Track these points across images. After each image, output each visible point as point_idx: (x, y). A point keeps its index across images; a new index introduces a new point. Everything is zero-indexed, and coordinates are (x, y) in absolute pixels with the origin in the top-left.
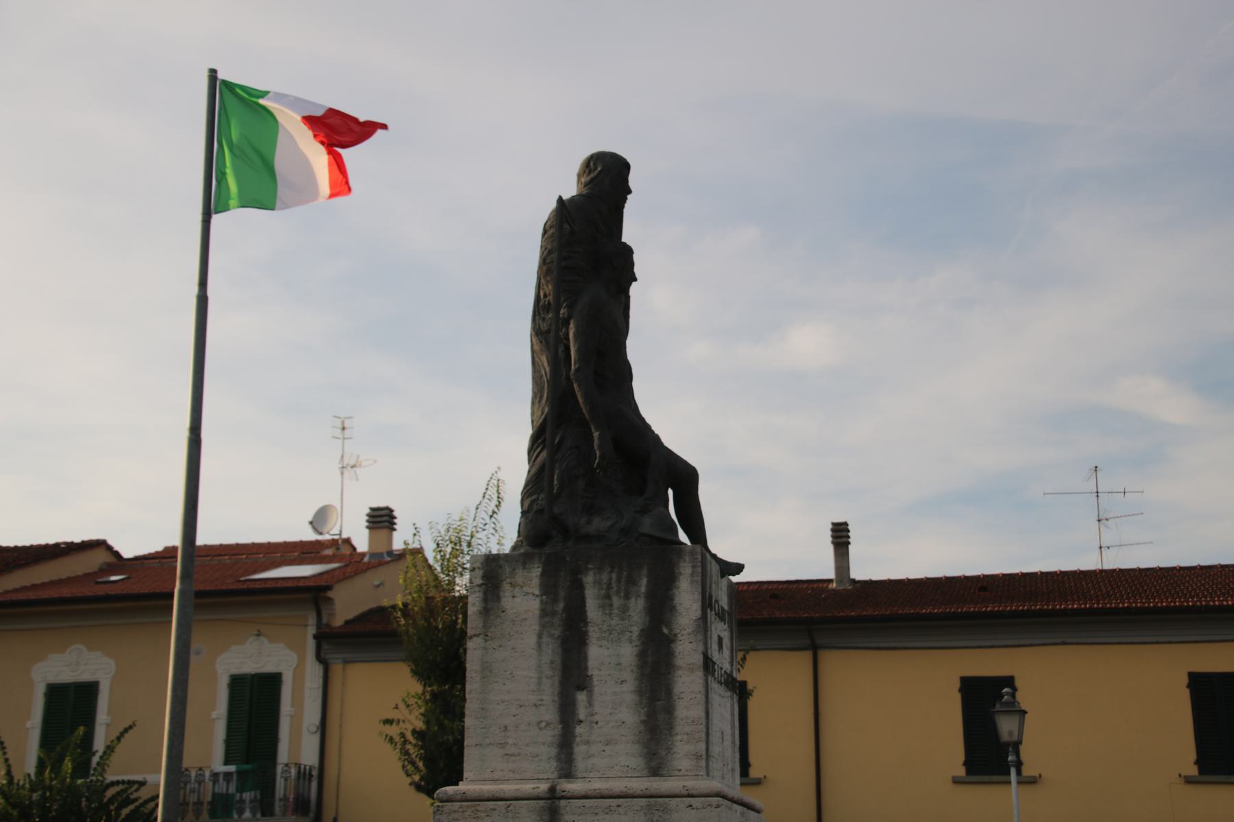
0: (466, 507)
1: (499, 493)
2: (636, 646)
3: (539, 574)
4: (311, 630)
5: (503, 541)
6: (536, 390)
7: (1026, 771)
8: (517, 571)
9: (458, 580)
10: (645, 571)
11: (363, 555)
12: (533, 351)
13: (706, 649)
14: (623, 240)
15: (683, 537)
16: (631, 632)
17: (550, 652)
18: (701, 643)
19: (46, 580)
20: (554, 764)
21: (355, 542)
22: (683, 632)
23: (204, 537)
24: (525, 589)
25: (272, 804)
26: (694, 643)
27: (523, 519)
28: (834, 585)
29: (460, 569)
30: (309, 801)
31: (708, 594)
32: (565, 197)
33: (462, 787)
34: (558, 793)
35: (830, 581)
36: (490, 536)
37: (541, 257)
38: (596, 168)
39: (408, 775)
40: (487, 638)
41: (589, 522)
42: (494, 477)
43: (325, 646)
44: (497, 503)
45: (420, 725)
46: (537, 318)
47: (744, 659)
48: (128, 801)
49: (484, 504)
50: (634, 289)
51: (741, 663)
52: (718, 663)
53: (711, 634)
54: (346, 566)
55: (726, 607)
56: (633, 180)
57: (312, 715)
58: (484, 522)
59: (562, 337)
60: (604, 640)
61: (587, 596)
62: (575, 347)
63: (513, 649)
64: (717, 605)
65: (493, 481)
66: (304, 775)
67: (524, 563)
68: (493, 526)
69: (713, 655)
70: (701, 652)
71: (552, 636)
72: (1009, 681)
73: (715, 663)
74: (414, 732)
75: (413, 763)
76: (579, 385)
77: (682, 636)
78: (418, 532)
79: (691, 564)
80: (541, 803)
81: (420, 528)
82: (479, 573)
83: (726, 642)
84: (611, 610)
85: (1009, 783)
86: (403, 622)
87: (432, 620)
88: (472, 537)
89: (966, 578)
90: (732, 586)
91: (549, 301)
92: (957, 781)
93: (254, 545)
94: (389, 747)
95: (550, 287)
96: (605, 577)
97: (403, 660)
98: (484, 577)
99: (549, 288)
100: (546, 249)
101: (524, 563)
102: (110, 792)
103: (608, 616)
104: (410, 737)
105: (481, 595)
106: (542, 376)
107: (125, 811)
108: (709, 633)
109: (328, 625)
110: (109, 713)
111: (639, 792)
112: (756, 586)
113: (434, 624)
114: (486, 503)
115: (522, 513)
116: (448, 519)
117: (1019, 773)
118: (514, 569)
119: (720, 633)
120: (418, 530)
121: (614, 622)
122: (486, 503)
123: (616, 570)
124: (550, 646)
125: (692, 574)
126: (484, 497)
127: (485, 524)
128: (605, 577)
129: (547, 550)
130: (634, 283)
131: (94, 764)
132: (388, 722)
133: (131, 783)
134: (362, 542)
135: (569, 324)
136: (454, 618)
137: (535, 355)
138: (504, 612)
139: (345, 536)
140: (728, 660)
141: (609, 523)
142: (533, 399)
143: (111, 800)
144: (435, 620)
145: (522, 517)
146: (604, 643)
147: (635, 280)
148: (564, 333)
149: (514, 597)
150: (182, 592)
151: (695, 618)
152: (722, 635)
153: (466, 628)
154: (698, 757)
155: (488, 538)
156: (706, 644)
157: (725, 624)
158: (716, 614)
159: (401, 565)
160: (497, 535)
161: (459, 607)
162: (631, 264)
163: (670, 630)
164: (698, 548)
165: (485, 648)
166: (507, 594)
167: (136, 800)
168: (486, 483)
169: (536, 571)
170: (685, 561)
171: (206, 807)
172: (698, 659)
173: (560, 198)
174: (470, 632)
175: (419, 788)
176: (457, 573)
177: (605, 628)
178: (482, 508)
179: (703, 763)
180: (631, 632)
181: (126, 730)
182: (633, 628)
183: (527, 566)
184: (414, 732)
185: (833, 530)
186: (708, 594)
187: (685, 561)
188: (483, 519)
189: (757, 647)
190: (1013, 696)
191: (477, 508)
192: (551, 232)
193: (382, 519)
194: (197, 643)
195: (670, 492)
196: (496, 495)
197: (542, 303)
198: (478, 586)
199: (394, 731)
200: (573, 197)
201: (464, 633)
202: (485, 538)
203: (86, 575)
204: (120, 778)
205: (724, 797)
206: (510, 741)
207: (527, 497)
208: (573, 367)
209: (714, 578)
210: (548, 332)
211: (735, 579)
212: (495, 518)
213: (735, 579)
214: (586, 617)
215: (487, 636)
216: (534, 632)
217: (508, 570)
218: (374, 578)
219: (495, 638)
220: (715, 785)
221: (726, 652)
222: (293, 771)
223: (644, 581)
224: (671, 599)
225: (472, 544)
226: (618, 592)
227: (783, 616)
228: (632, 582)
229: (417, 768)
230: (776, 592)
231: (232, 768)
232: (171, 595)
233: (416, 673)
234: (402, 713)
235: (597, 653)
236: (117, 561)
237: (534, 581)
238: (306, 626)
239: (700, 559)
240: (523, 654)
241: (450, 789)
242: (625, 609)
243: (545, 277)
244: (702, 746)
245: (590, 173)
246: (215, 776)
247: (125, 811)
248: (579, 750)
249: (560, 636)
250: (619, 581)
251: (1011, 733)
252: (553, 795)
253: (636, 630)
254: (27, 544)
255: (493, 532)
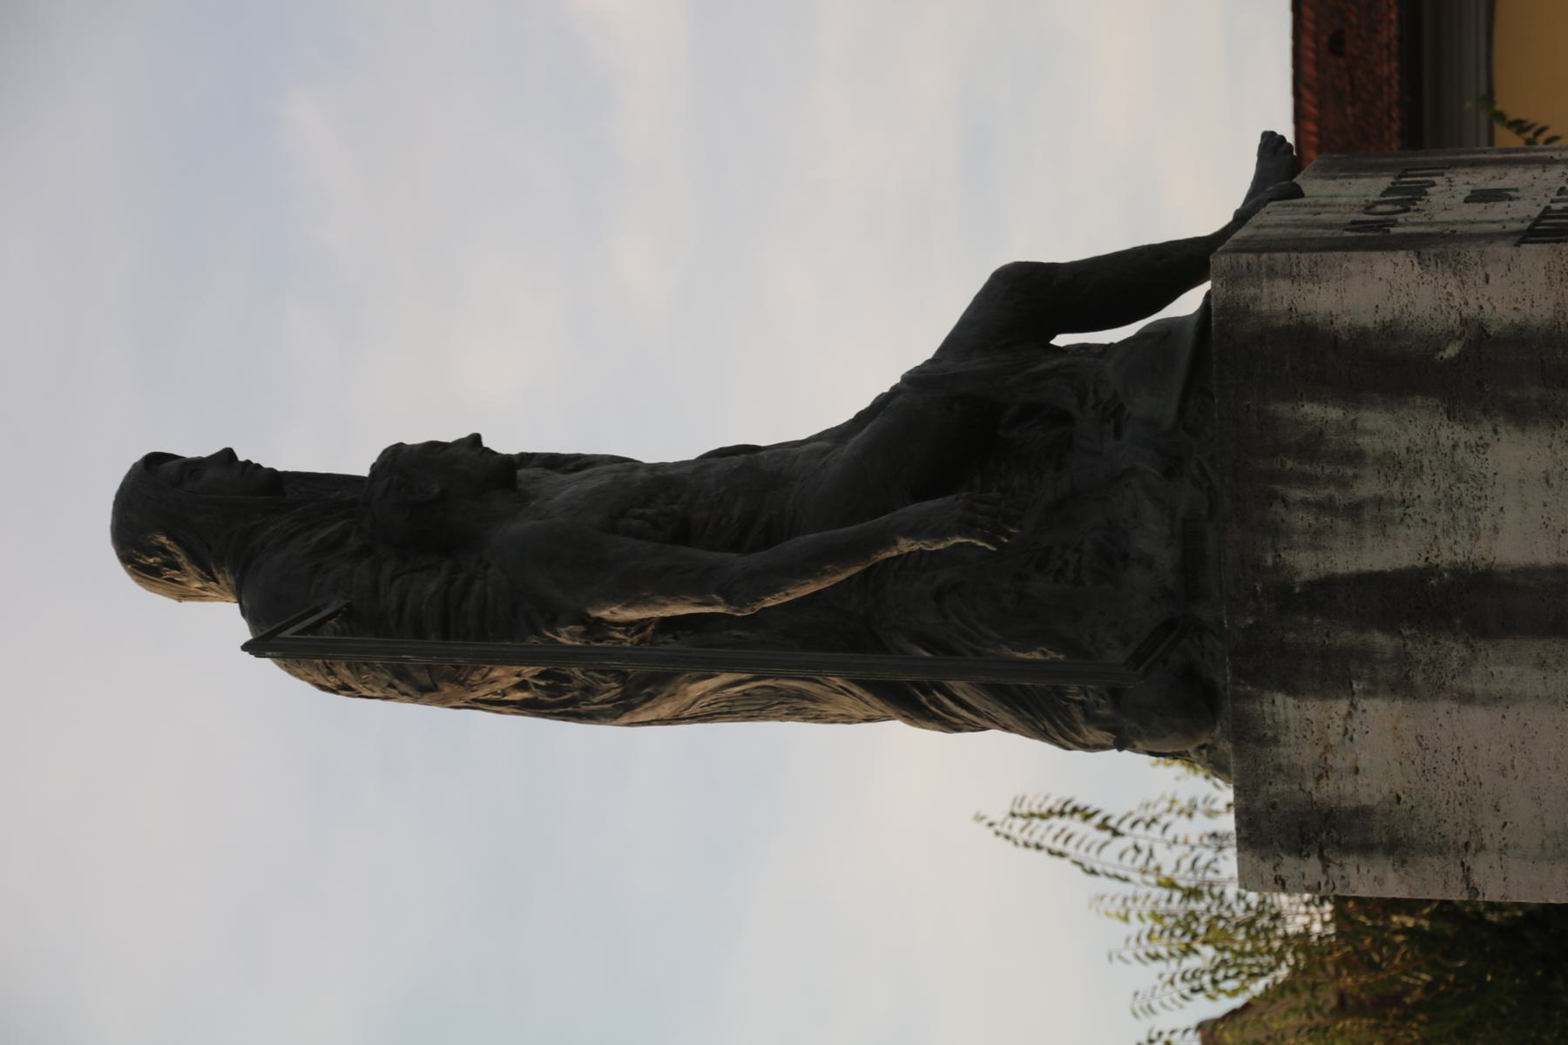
0: (1090, 906)
1: (1050, 813)
2: (1495, 431)
3: (1290, 701)
5: (1183, 802)
6: (784, 709)
8: (1284, 762)
9: (1295, 925)
10: (1283, 409)
13: (1505, 235)
14: (365, 472)
15: (1188, 303)
16: (1455, 446)
17: (1511, 671)
18: (1489, 249)
22: (1457, 301)
24: (1334, 739)
26: (1489, 270)
27: (1139, 745)
29: (1265, 921)
31: (1348, 234)
32: (247, 636)
36: (1169, 835)
37: (415, 700)
38: (162, 549)
40: (1473, 845)
42: (1005, 830)
44: (1077, 817)
46: (584, 708)
47: (1519, 126)
49: (1080, 854)
50: (503, 442)
51: (1530, 135)
52: (1546, 202)
53: (1464, 223)
55: (1386, 181)
56: (195, 445)
58: (1132, 853)
59: (636, 638)
60: (1477, 519)
61: (1353, 568)
62: (664, 605)
63: (1503, 772)
64: (1380, 208)
65: (1015, 832)
67: (1261, 741)
68: (1140, 827)
69: (1523, 215)
70: (1514, 250)
71: (1465, 666)
73: (1548, 208)
76: (770, 592)
77: (1466, 303)
78: (1160, 1034)
79: (1265, 283)
81: (1150, 1032)
82: (1290, 866)
83: (1484, 179)
84: (1392, 502)
87: (1408, 1000)
88: (1171, 885)
91: (541, 676)
95: (497, 673)
96: (1301, 520)
98: (1300, 852)
99: (504, 677)
100: (391, 686)
101: (1261, 741)
103: (1410, 511)
105: (1351, 861)
106: (745, 694)
108: (1459, 228)
112: (1307, 95)
113: (1417, 993)
114: (1078, 846)
115: (1120, 749)
116: (1127, 962)
118: (1279, 768)
119: (1461, 198)
120: (1154, 1036)
121: (1427, 494)
122: (1078, 846)
123: (1278, 487)
124: (1495, 669)
125: (1293, 277)
126: (1061, 855)
127: (1137, 849)
128: (1301, 520)
130: (486, 443)
135: (600, 620)
136: (1400, 938)
137: (686, 714)
138: (1399, 798)
140: (1537, 172)
142: (805, 720)
144: (1408, 988)
145: (1134, 749)
146: (1485, 521)
147: (476, 439)
148: (625, 632)
149: (1357, 770)
151: (1417, 268)
152: (1466, 191)
153: (1429, 902)
155: (1175, 842)
156: (1490, 237)
157: (1433, 184)
158: (1407, 210)
160: (1164, 820)
161: (1369, 923)
163: (1450, 336)
164: (1219, 261)
165: (1503, 850)
166: (1349, 789)
168: (1022, 851)
169: (1284, 708)
170: (1255, 299)
173: (247, 647)
174: (1457, 894)
176: (1275, 927)
177: (1443, 518)
178: (1091, 859)
180: (1455, 446)
182: (1443, 440)
183: (1270, 733)
186: (1348, 234)
187: (1255, 299)
188: (1121, 856)
189: (1483, 90)
191: (1093, 872)
192: (345, 674)
195: (1061, 340)
196: (1055, 820)
197: (542, 696)
198: (1325, 870)
200: (243, 613)
201: (1445, 910)
202: (1179, 850)
207: (1079, 733)
208: (720, 610)
209: (1302, 215)
210: (622, 676)
212: (1120, 822)
214: (1413, 570)
215: (1467, 845)
216: (1455, 715)
217: (1279, 787)
219: (1473, 823)
221: (1513, 178)
223: (1312, 411)
224: (1362, 334)
225: (1193, 884)
226: (1343, 484)
227: (1393, 17)
228: (1312, 445)
230: (1325, 39)
237: (1311, 714)
239: (1251, 257)
240: (1518, 744)
242: (1390, 464)
243: (471, 688)
245: (177, 567)
249: (1466, 643)
250: (1308, 481)
253: (1450, 433)
255: (1156, 829)
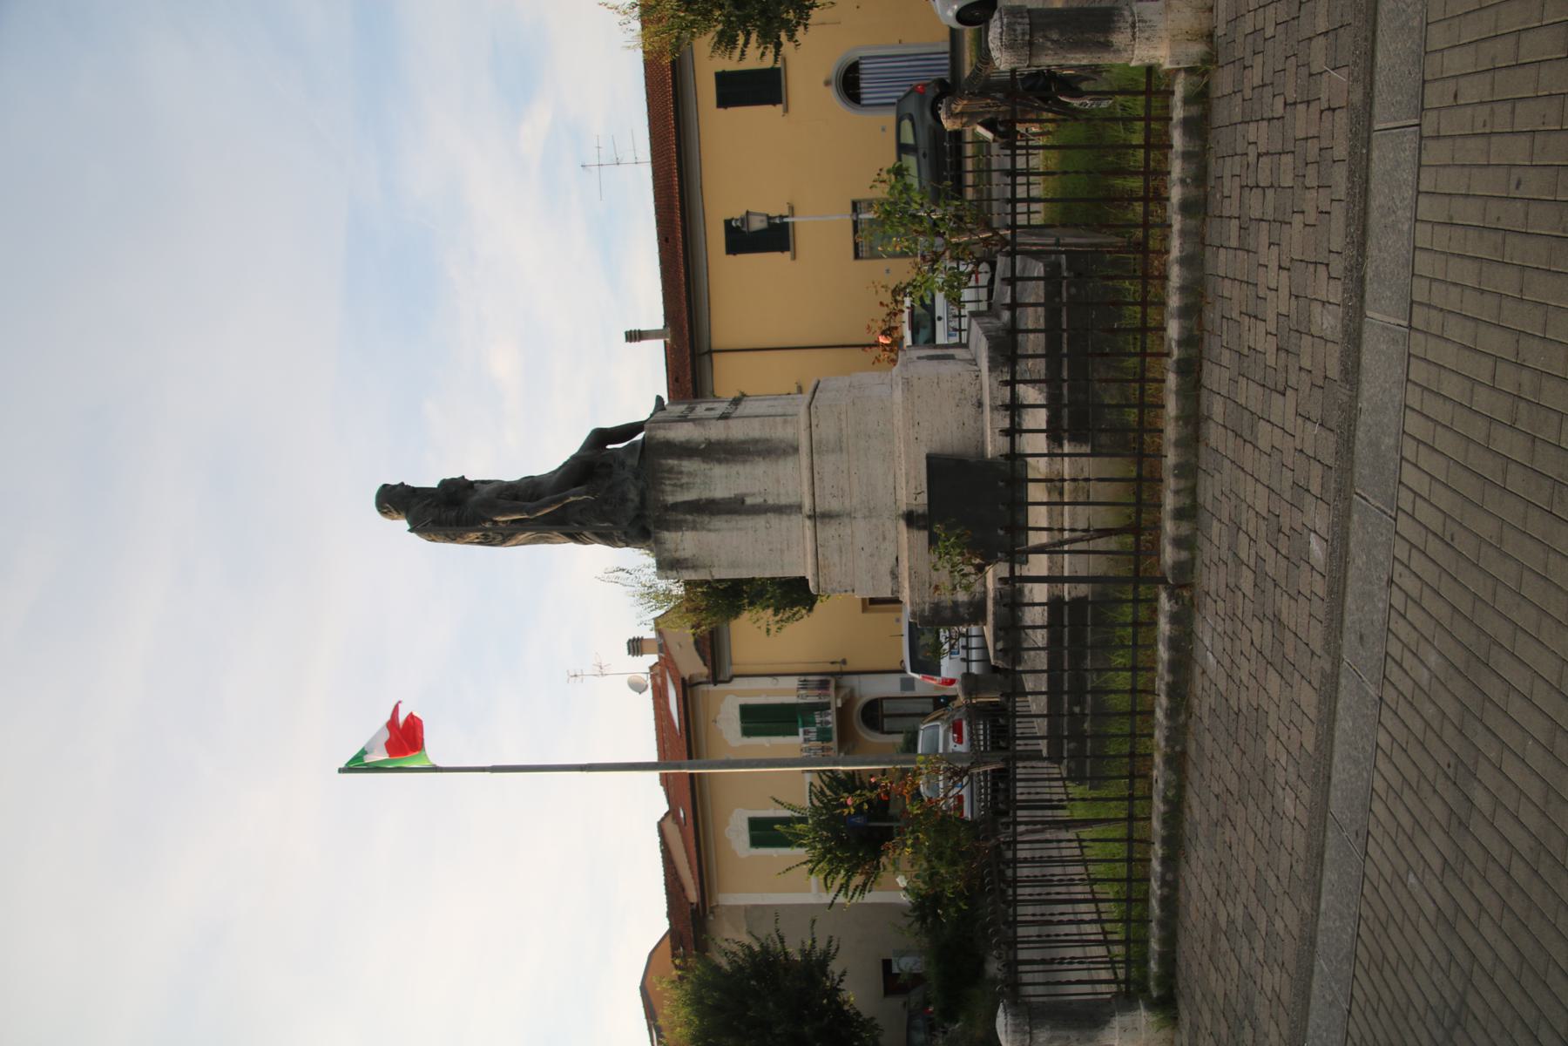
4: (711, 687)
7: (786, 212)
10: (663, 462)
11: (660, 658)
12: (516, 545)
15: (639, 437)
19: (684, 855)
20: (793, 517)
21: (652, 664)
23: (653, 757)
25: (823, 703)
28: (668, 340)
30: (821, 681)
33: (809, 577)
34: (812, 513)
35: (665, 342)
39: (802, 617)
41: (632, 501)
43: (721, 678)
45: (770, 611)
48: (822, 792)
50: (471, 477)
54: (668, 668)
55: (686, 406)
57: (766, 683)
66: (804, 685)
72: (728, 223)
74: (775, 615)
75: (794, 614)
80: (818, 524)
82: (669, 573)
83: (709, 405)
85: (793, 223)
86: (704, 628)
89: (660, 251)
90: (671, 403)
92: (794, 257)
93: (658, 739)
94: (784, 630)
97: (728, 625)
99: (473, 536)
102: (817, 803)
104: (778, 618)
107: (828, 792)
109: (707, 677)
110: (767, 809)
111: (809, 460)
117: (787, 217)
128: (668, 488)
129: (652, 528)
131: (800, 815)
132: (768, 631)
133: (811, 791)
134: (653, 658)
139: (648, 671)
141: (632, 488)
143: (821, 802)
146: (712, 488)
147: (463, 477)
150: (689, 768)
154: (785, 422)
159: (667, 631)
162: (453, 480)
164: (646, 426)
167: (821, 787)
169: (666, 535)
171: (825, 744)
172: (721, 423)
175: (810, 610)
179: (789, 418)
181: (777, 801)
184: (775, 615)
185: (631, 341)
190: (737, 220)
193: (636, 646)
194: (723, 757)
199: (773, 628)
203: (680, 831)
204: (808, 798)
205: (810, 404)
206: (779, 546)
211: (666, 401)
213: (666, 401)
217: (666, 554)
218: (675, 650)
220: (803, 410)
221: (716, 405)
222: (802, 692)
224: (681, 443)
228: (671, 470)
229: (798, 612)
231: (801, 730)
232: (692, 775)
233: (737, 615)
234: (762, 623)
235: (720, 492)
236: (672, 813)
238: (708, 691)
241: (811, 585)
242: (690, 474)
244: (778, 418)
246: (806, 741)
247: (828, 792)
248: (784, 501)
250: (670, 479)
251: (762, 221)
252: (813, 517)
253: (704, 466)
254: (663, 878)
